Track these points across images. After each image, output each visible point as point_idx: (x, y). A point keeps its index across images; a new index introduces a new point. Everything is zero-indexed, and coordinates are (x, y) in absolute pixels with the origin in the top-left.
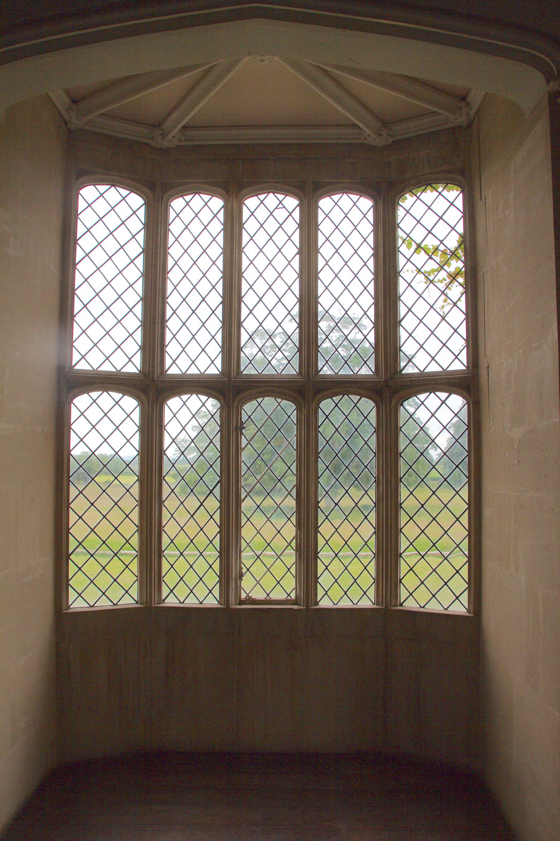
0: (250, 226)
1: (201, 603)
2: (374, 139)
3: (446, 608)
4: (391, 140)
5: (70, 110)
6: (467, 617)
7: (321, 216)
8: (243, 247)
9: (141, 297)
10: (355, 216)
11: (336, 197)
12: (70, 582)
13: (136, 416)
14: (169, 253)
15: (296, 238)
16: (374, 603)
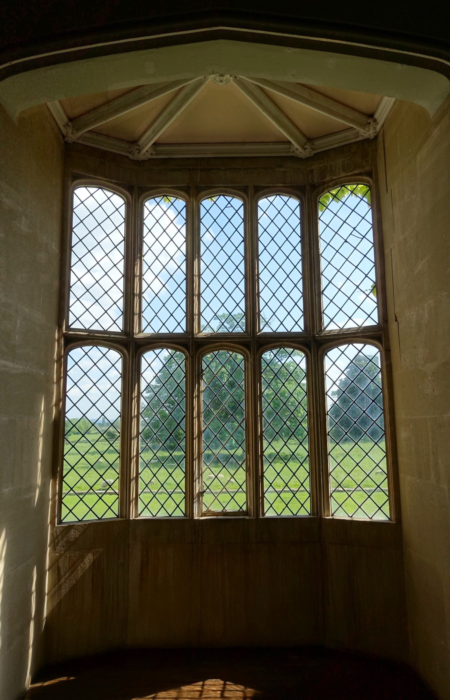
0: (206, 221)
1: (170, 516)
2: (301, 153)
3: (370, 517)
4: (313, 153)
5: (67, 127)
6: (184, 520)
7: (260, 213)
8: (201, 236)
9: (123, 274)
10: (286, 212)
11: (271, 198)
12: (63, 501)
13: (119, 365)
14: (144, 241)
15: (241, 230)
16: (310, 513)
